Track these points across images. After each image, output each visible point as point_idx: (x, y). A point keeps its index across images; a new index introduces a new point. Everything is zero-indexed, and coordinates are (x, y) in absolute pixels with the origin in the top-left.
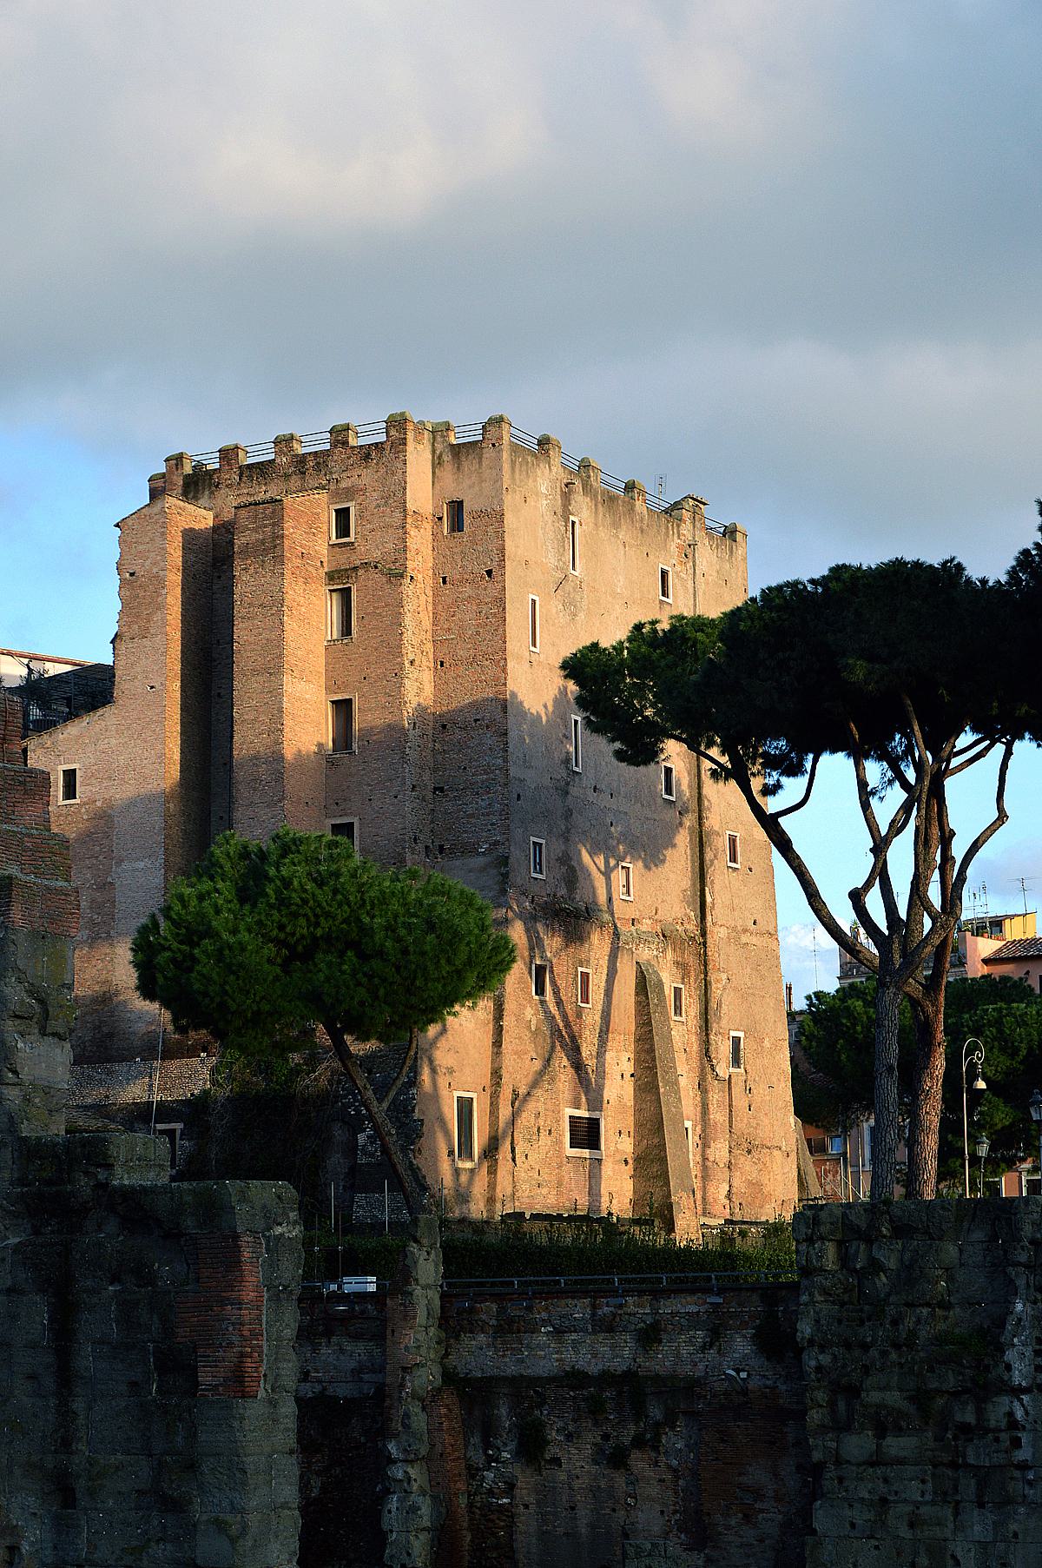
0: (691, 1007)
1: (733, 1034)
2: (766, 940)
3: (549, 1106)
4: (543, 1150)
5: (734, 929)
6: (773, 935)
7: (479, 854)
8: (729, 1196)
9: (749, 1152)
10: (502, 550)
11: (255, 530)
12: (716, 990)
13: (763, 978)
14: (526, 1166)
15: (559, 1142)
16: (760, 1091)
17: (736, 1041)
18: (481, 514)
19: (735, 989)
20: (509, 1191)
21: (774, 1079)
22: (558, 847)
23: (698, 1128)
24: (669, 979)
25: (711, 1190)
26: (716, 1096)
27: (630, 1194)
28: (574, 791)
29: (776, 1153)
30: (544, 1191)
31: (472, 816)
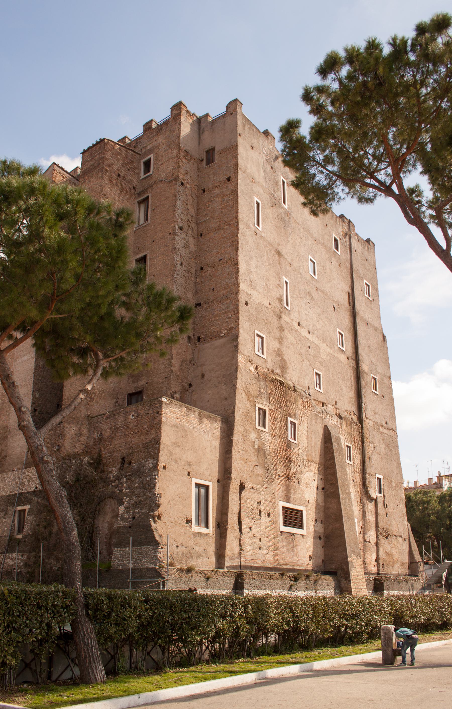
0: (357, 459)
1: (378, 476)
2: (391, 433)
3: (268, 498)
4: (263, 527)
5: (376, 423)
6: (394, 431)
7: (221, 337)
8: (377, 560)
9: (387, 538)
10: (236, 165)
11: (91, 160)
12: (369, 451)
13: (391, 451)
14: (250, 535)
15: (274, 522)
16: (391, 506)
17: (379, 479)
18: (223, 151)
19: (378, 453)
20: (236, 550)
21: (398, 502)
22: (276, 346)
23: (361, 524)
24: (345, 441)
25: (368, 556)
26: (370, 507)
27: (182, 116)
28: (285, 318)
29: (400, 539)
30: (265, 552)
31: (217, 315)
